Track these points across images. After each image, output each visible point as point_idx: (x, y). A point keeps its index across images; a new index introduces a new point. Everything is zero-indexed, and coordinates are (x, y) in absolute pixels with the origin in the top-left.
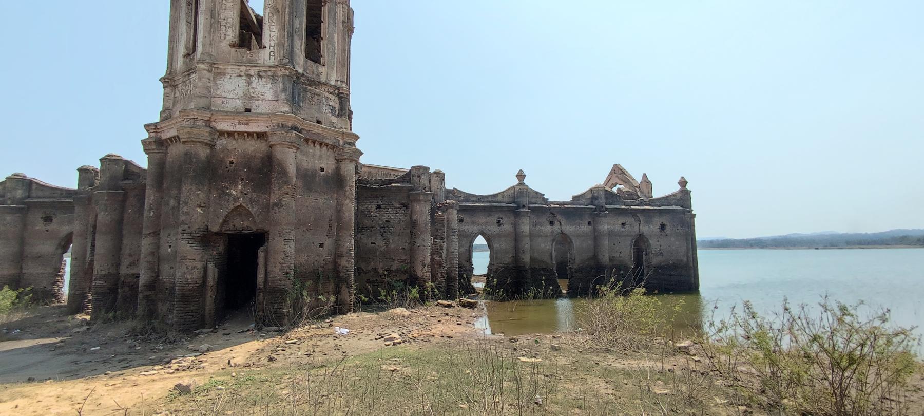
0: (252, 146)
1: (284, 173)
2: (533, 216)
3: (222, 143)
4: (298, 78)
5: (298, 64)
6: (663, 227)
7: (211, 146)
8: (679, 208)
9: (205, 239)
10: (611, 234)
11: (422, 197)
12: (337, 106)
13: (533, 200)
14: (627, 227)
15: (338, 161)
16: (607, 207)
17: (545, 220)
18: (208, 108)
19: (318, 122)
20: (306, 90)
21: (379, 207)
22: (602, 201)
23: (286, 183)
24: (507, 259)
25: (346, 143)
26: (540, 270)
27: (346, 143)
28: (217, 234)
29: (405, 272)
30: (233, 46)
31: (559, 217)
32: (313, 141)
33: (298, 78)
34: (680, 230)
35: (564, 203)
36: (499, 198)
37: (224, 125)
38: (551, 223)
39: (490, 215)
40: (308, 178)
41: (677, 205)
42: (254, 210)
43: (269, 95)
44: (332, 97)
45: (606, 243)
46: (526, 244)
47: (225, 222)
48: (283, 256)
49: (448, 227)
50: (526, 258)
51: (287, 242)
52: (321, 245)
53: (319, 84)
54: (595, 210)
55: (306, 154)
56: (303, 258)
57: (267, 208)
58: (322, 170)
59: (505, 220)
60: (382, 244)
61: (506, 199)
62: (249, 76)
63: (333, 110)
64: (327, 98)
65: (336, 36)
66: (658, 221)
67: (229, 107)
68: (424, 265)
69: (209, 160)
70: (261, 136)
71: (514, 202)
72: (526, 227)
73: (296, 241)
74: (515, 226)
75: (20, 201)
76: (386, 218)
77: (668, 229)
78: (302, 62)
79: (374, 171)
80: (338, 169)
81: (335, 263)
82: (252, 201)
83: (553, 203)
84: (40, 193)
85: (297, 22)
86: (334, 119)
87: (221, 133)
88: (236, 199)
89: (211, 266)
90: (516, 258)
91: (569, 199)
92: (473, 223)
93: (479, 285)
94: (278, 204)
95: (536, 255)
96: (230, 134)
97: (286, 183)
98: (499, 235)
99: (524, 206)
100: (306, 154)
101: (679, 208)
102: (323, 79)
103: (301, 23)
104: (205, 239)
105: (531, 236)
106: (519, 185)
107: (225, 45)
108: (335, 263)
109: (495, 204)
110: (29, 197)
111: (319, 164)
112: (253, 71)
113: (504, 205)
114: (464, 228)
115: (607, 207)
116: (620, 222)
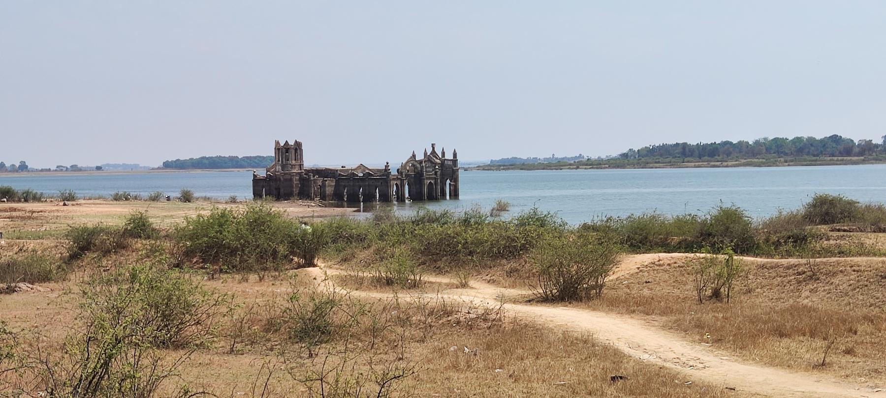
40: (286, 180)
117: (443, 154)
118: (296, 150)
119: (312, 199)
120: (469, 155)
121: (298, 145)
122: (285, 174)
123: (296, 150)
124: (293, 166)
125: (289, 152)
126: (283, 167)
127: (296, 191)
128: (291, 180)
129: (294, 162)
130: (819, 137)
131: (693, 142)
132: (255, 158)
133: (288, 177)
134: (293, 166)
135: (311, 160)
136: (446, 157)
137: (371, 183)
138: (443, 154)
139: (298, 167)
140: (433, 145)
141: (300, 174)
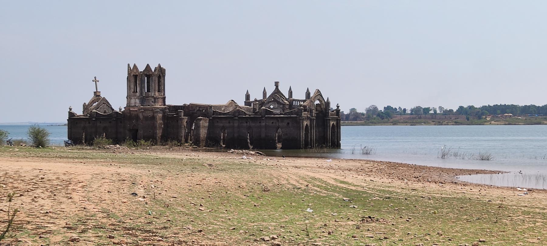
0: (136, 113)
6: (288, 123)
8: (295, 116)
9: (130, 130)
10: (266, 127)
14: (274, 124)
18: (129, 106)
37: (131, 109)
38: (247, 122)
40: (146, 118)
48: (141, 132)
50: (263, 136)
66: (286, 121)
73: (277, 132)
77: (290, 125)
101: (295, 116)
104: (130, 130)
117: (291, 93)
118: (159, 77)
119: (247, 148)
120: (342, 100)
121: (161, 72)
122: (146, 110)
123: (159, 77)
124: (155, 99)
125: (147, 81)
126: (143, 99)
127: (159, 133)
128: (153, 118)
129: (157, 93)
130: (492, 105)
131: (478, 105)
132: (420, 123)
133: (150, 114)
134: (155, 99)
135: (176, 95)
136: (294, 97)
137: (270, 123)
138: (291, 93)
139: (161, 100)
140: (277, 84)
141: (163, 110)
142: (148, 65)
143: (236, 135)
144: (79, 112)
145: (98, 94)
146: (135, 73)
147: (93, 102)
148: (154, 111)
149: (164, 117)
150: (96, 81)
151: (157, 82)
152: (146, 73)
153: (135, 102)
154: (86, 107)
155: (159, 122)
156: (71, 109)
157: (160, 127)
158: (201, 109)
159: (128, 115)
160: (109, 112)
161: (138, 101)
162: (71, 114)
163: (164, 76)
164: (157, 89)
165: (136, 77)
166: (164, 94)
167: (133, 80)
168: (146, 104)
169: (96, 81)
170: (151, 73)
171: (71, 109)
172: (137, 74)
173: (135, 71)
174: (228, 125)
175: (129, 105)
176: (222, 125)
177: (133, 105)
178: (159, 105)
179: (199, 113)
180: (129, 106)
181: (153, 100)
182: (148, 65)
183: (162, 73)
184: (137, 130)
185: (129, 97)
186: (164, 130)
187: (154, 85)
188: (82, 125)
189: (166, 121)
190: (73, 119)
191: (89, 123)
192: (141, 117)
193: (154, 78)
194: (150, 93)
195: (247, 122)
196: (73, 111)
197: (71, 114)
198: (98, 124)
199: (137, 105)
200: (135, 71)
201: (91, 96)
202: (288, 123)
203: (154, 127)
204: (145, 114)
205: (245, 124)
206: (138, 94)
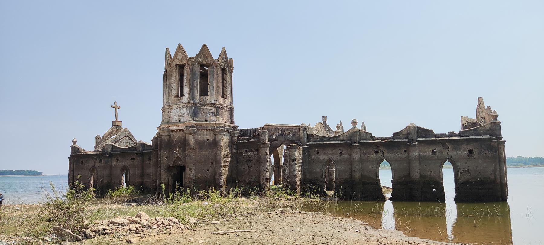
0: (181, 134)
1: (189, 144)
2: (363, 148)
3: (173, 133)
4: (196, 105)
5: (196, 99)
6: (471, 152)
7: (169, 135)
8: (488, 136)
9: (169, 169)
10: (421, 159)
11: (262, 146)
12: (215, 112)
13: (364, 138)
14: (437, 154)
15: (215, 135)
16: (419, 139)
17: (371, 150)
18: (168, 122)
19: (206, 121)
20: (200, 109)
21: (246, 151)
22: (414, 135)
23: (190, 148)
24: (346, 176)
25: (217, 127)
26: (368, 183)
27: (217, 127)
28: (173, 167)
29: (257, 182)
30: (176, 97)
31: (381, 148)
32: (204, 128)
33: (196, 105)
34: (488, 153)
35: (386, 138)
36: (341, 138)
37: (172, 128)
38: (377, 152)
39: (335, 149)
40: (201, 145)
41: (486, 134)
42: (182, 158)
43: (186, 115)
44: (213, 108)
45: (416, 165)
46: (357, 166)
47: (174, 162)
48: (190, 173)
49: (290, 158)
50: (357, 175)
51: (190, 170)
52: (208, 170)
53: (206, 105)
54: (408, 142)
55: (200, 135)
56: (200, 175)
57: (185, 157)
58: (208, 140)
59: (344, 151)
60: (248, 168)
61: (345, 138)
62: (180, 108)
63: (213, 113)
64: (210, 110)
65: (214, 81)
66: (466, 148)
67: (174, 121)
68: (264, 179)
69: (169, 141)
70: (182, 130)
71: (350, 140)
72: (356, 156)
74: (350, 155)
75: (141, 152)
76: (249, 156)
77: (476, 153)
78: (198, 98)
79: (270, 127)
80: (215, 138)
81: (214, 177)
82: (181, 155)
83: (378, 139)
84: (147, 148)
85: (195, 83)
86: (214, 118)
87: (172, 131)
88: (177, 154)
89: (170, 178)
90: (351, 176)
91: (390, 135)
92: (325, 154)
93: (388, 195)
94: (187, 156)
95: (365, 173)
96: (174, 131)
97: (190, 148)
98: (341, 161)
99: (355, 143)
100: (200, 135)
101: (488, 136)
102: (208, 102)
103: (197, 83)
104: (169, 169)
105: (361, 161)
106: (353, 129)
107: (173, 97)
108: (214, 177)
109: (338, 142)
110: (144, 150)
111: (206, 138)
112: (181, 106)
113: (343, 142)
114: (319, 157)
115: (419, 139)
116: (431, 150)
121: (226, 67)
122: (200, 128)
123: (224, 71)
126: (195, 110)
127: (225, 171)
128: (215, 144)
133: (209, 136)
135: (253, 107)
137: (428, 151)
139: (226, 113)
142: (204, 46)
143: (357, 175)
144: (88, 146)
145: (118, 124)
146: (180, 61)
147: (110, 134)
148: (215, 131)
149: (232, 144)
150: (115, 107)
151: (220, 78)
152: (200, 60)
153: (181, 114)
154: (99, 142)
155: (225, 151)
156: (74, 143)
157: (226, 162)
158: (285, 133)
159: (166, 138)
160: (130, 145)
161: (185, 112)
162: (75, 150)
163: (231, 71)
164: (220, 91)
165: (181, 67)
166: (231, 103)
167: (175, 74)
168: (200, 117)
169: (115, 107)
170: (209, 61)
171: (74, 143)
172: (184, 61)
173: (180, 57)
174: (338, 157)
175: (167, 122)
176: (326, 158)
177: (176, 119)
178: (223, 120)
179: (281, 139)
180: (168, 122)
181: (214, 110)
182: (204, 46)
183: (228, 66)
184: (182, 169)
185: (166, 108)
186: (231, 166)
187: (214, 83)
188: (90, 165)
189: (235, 151)
190: (77, 158)
191: (101, 161)
192: (192, 142)
193: (215, 70)
194: (208, 98)
195: (377, 152)
196: (77, 145)
197: (75, 150)
198: (114, 163)
199: (183, 119)
200: (180, 57)
201: (109, 127)
202: (471, 152)
203: (216, 162)
204: (199, 138)
205: (374, 156)
206: (185, 99)
